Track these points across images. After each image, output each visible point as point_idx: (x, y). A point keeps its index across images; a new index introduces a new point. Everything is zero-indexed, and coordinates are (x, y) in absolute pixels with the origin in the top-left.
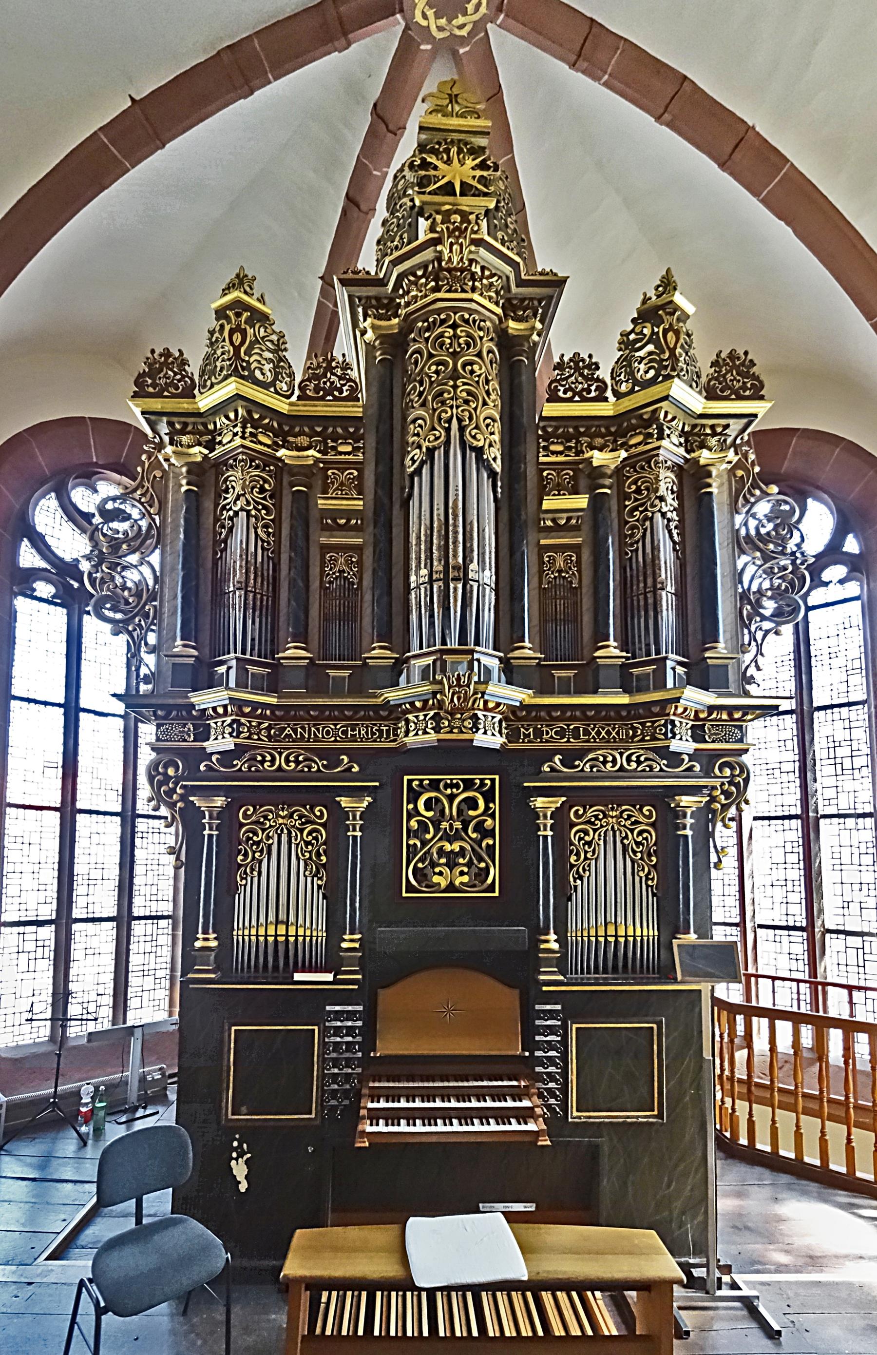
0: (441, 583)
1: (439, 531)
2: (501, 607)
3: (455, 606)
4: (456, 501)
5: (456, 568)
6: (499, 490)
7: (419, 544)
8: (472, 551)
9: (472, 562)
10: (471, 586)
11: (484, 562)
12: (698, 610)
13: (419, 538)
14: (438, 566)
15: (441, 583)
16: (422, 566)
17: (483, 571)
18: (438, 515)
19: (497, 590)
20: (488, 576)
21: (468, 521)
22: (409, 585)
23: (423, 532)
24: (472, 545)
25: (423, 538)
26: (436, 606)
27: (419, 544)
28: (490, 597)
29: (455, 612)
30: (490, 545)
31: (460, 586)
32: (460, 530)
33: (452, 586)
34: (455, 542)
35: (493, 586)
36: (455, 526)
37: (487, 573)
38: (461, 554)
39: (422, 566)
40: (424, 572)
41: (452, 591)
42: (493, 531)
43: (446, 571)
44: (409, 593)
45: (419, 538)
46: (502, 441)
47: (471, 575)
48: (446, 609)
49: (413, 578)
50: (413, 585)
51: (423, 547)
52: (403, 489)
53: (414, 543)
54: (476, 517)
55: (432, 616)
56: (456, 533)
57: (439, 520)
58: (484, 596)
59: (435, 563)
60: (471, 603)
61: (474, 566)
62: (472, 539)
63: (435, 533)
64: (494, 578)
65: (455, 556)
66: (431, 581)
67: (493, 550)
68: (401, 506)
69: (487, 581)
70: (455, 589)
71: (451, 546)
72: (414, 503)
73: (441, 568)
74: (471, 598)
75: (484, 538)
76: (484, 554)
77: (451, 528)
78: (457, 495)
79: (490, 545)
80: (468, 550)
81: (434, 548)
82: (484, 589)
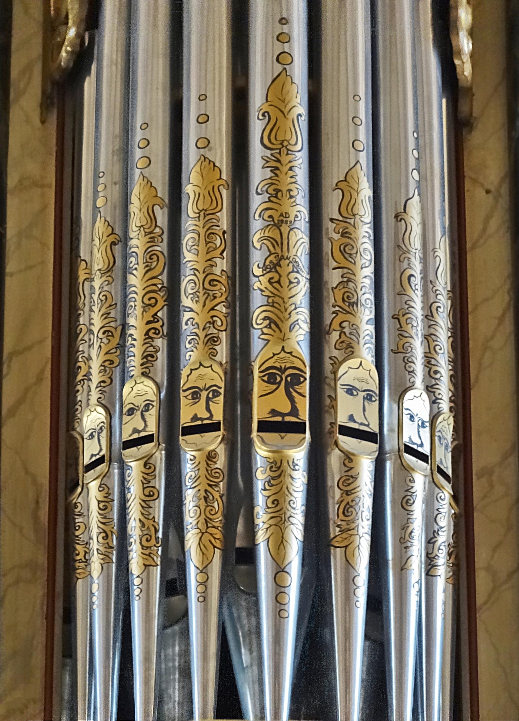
0: (214, 442)
1: (207, 215)
2: (482, 555)
3: (279, 543)
4: (279, 82)
5: (279, 376)
6: (465, 44)
7: (118, 270)
8: (350, 303)
9: (349, 349)
10: (348, 458)
11: (402, 351)
12: (392, 672)
13: (120, 240)
14: (203, 368)
15: (214, 442)
16: (134, 362)
17: (401, 392)
18: (205, 143)
19: (462, 480)
20: (420, 416)
21: (332, 175)
22: (73, 448)
23: (137, 218)
24: (348, 280)
25: (137, 242)
26: (191, 539)
27: (118, 270)
28: (429, 510)
29: (279, 570)
30: (428, 283)
31: (299, 455)
32: (300, 209)
33: (261, 453)
34: (276, 264)
35: (445, 459)
36: (276, 193)
37: (417, 403)
38: (302, 316)
39: (134, 362)
40: (140, 390)
41: (261, 477)
42: (441, 222)
43: (237, 393)
44: (73, 484)
45: (120, 240)
46: (183, 338)
47: (347, 409)
48: (240, 559)
49: (91, 418)
50: (90, 450)
51: (136, 280)
52: (53, 26)
53: (99, 262)
54: (364, 159)
55: (174, 586)
56: (279, 222)
57: (208, 164)
58: (404, 503)
59: (190, 354)
60: (348, 530)
61: (358, 369)
62: (348, 251)
63: (190, 224)
64: (447, 425)
65: (277, 324)
66: (172, 433)
67: (444, 303)
68: (46, 104)
69: (411, 433)
70: (279, 469)
71: (259, 282)
72: (101, 89)
73: (215, 377)
74: (348, 509)
75: (401, 249)
76: (401, 317)
77: (257, 202)
78: (283, 58)
79: (428, 283)
80: (331, 301)
81: (187, 284)
82: (405, 470)
